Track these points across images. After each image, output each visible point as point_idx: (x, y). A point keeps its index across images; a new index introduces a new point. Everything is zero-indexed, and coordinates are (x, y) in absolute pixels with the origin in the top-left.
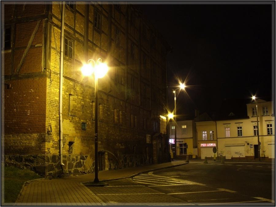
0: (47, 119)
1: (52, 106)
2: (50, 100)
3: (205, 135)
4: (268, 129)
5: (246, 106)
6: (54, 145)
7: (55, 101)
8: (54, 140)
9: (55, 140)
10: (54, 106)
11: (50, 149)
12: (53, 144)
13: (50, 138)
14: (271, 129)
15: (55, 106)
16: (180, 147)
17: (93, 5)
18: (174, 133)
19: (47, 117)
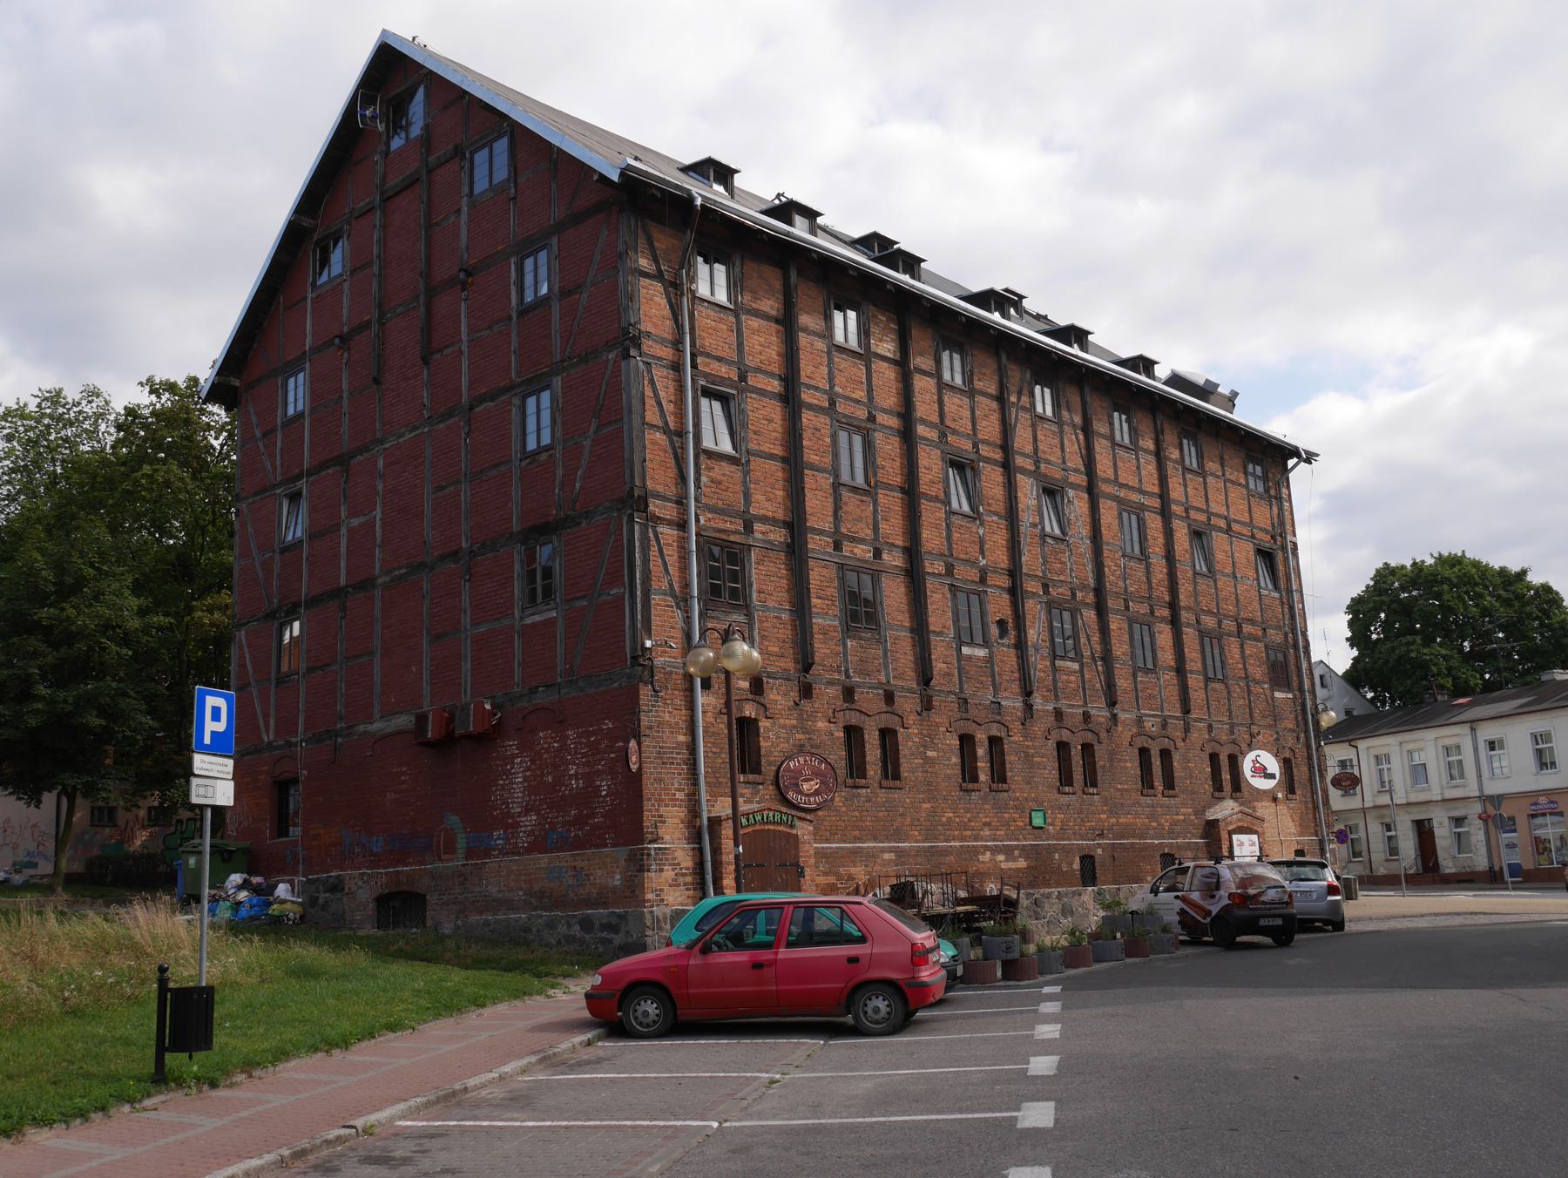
0: (647, 805)
1: (663, 763)
2: (655, 747)
3: (1019, 400)
4: (1381, 771)
5: (1041, 1164)
6: (681, 880)
7: (675, 748)
8: (679, 864)
9: (683, 865)
10: (673, 763)
11: (661, 890)
12: (676, 875)
13: (662, 859)
14: (1460, 762)
15: (678, 764)
16: (1400, 883)
17: (621, 430)
18: (728, 790)
19: (649, 799)
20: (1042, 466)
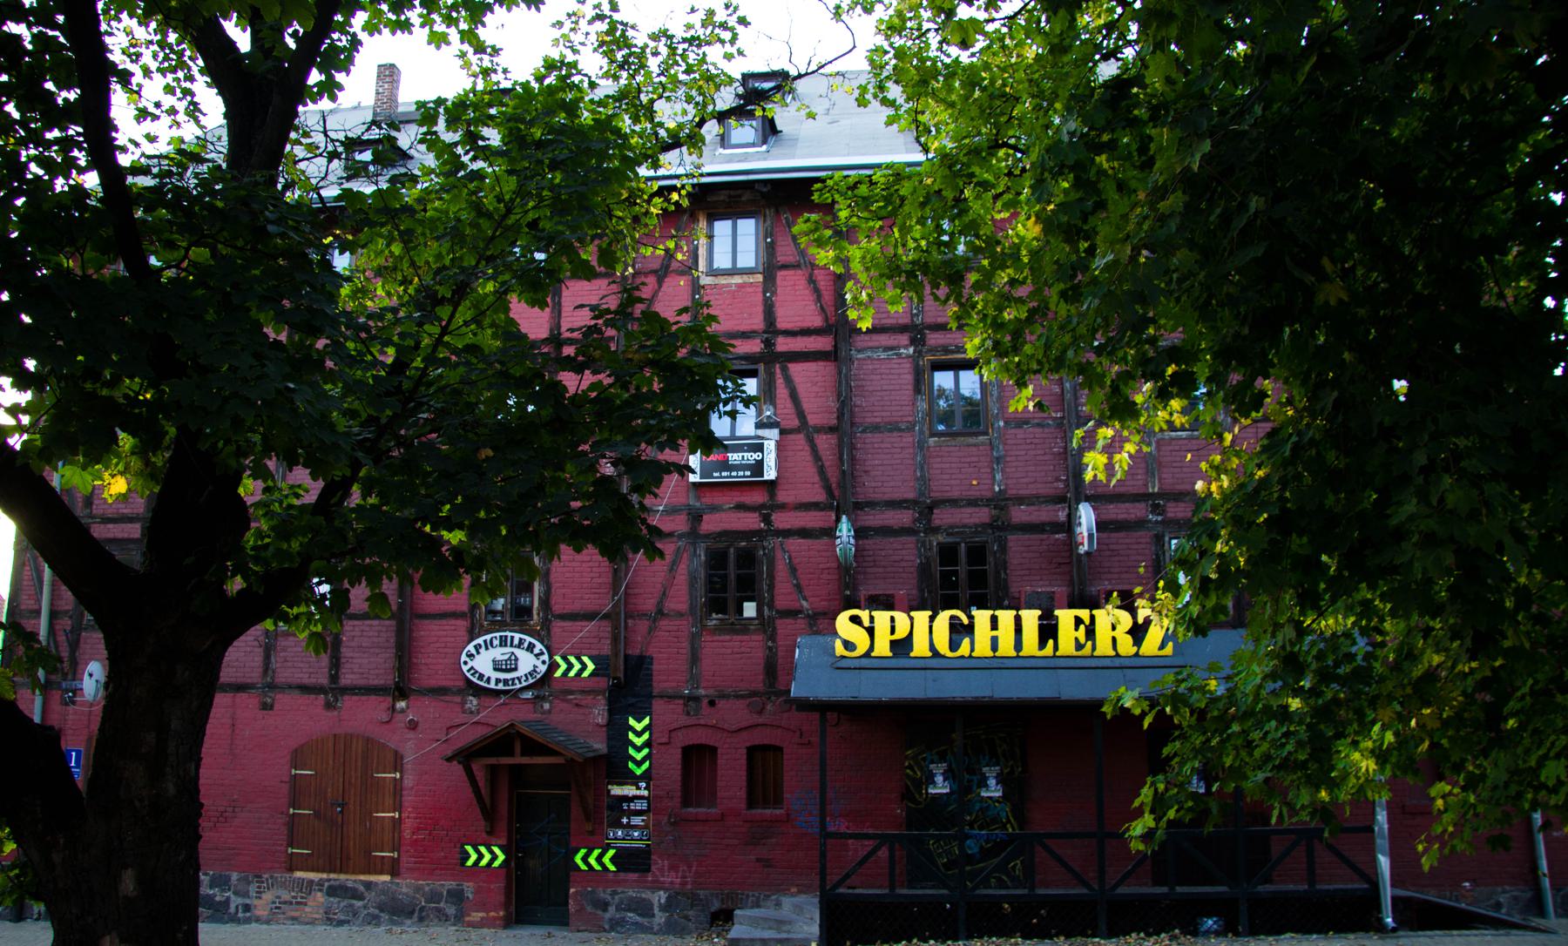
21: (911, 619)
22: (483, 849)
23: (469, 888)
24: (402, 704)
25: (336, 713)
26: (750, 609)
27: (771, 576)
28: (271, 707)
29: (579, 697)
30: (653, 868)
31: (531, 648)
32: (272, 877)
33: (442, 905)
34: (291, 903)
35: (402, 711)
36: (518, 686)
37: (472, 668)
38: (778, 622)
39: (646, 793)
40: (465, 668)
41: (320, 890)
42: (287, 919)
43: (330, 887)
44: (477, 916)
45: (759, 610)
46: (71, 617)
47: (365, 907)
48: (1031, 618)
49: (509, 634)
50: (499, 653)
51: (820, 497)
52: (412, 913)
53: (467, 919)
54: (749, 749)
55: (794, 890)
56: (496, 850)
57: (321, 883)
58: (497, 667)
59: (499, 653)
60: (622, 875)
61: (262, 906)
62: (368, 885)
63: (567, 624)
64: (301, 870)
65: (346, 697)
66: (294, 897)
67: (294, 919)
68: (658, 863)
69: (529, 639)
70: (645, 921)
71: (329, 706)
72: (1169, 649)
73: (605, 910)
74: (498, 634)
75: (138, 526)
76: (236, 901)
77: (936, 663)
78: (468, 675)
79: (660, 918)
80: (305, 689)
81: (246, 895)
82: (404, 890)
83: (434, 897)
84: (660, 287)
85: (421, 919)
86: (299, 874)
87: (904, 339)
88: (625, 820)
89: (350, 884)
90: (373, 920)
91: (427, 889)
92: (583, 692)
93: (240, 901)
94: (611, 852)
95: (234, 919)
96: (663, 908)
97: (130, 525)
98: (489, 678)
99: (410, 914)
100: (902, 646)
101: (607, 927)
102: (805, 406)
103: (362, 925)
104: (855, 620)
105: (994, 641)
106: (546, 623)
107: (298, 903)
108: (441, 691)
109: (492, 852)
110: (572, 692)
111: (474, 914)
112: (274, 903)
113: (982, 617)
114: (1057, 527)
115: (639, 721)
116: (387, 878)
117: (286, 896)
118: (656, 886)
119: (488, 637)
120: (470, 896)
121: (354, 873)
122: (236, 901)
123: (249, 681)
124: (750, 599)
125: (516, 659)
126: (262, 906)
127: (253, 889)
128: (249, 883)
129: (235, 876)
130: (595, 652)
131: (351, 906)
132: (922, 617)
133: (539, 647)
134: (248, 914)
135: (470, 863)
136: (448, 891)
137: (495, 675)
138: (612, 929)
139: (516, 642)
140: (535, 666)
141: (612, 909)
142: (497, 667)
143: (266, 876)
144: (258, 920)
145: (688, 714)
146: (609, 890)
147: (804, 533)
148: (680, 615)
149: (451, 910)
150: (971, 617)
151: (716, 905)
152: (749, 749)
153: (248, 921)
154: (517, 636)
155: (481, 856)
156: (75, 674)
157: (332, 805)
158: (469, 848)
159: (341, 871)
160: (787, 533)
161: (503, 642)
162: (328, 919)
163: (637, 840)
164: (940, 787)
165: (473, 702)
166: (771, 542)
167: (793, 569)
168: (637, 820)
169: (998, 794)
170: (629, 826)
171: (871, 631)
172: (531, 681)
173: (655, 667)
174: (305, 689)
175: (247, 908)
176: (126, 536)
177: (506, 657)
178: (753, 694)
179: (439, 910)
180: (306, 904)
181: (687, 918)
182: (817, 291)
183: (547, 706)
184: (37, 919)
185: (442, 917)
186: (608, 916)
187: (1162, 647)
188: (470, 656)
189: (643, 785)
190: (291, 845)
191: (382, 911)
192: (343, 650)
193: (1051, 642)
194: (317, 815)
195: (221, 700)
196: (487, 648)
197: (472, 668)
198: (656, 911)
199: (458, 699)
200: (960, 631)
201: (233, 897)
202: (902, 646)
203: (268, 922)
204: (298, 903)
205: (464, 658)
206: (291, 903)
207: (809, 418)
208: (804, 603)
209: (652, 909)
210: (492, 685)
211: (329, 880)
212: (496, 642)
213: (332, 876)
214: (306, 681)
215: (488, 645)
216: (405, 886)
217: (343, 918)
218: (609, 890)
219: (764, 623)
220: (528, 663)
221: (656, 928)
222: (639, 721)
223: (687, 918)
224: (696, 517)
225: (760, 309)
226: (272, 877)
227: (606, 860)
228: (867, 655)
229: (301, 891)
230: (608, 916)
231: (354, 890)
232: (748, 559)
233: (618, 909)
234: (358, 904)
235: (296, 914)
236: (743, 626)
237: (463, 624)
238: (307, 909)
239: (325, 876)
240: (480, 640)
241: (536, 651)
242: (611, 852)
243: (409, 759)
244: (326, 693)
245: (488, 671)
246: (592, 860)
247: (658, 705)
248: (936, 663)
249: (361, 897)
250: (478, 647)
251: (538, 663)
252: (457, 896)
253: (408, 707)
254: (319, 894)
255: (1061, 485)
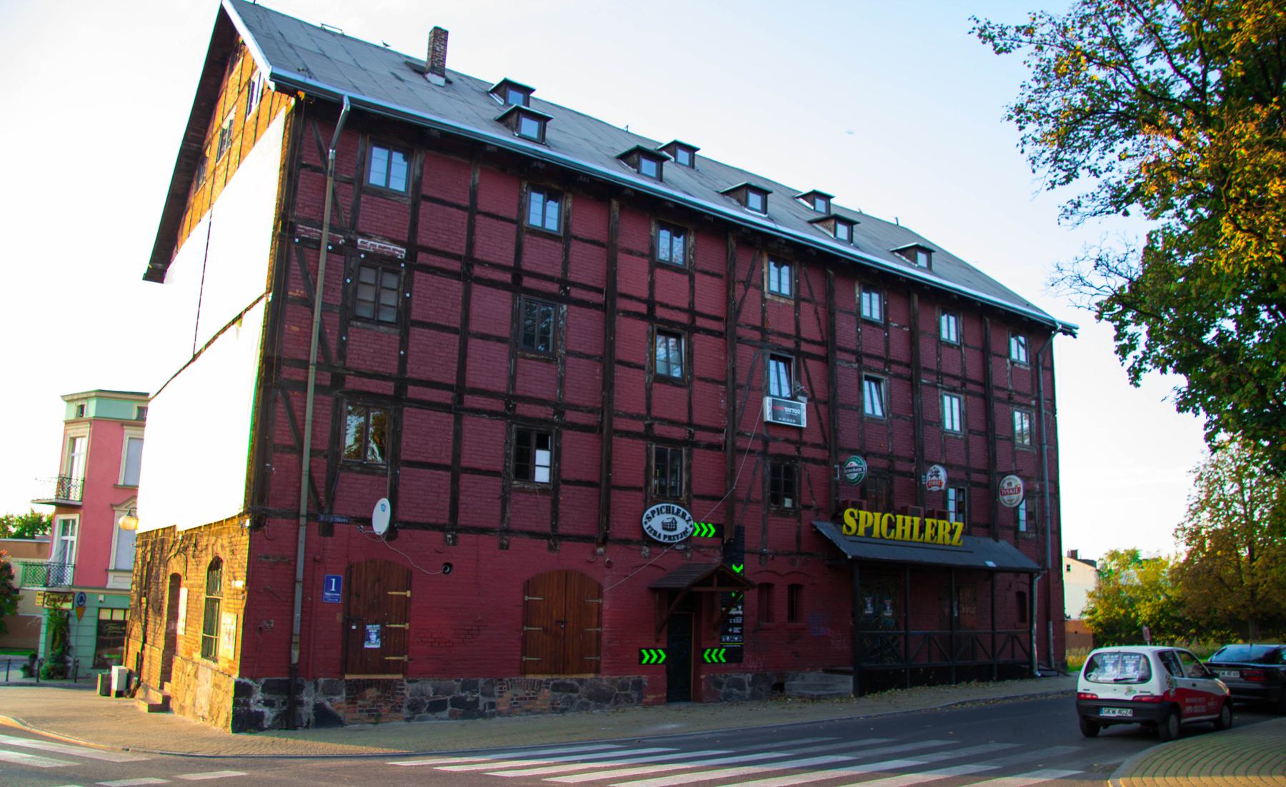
20: (803, 344)
21: (874, 517)
22: (652, 652)
23: (645, 678)
24: (601, 550)
25: (556, 554)
26: (788, 503)
27: (800, 484)
28: (507, 548)
29: (706, 550)
30: (744, 659)
31: (683, 516)
32: (511, 680)
33: (629, 692)
34: (526, 699)
35: (601, 554)
36: (677, 541)
37: (650, 527)
38: (803, 512)
39: (741, 613)
40: (645, 527)
41: (547, 688)
42: (523, 711)
43: (555, 684)
44: (650, 698)
45: (794, 504)
46: (326, 457)
47: (579, 697)
48: (917, 520)
49: (672, 505)
50: (665, 518)
51: (820, 441)
52: (610, 699)
53: (644, 700)
54: (789, 586)
55: (808, 669)
56: (661, 652)
57: (547, 683)
58: (665, 527)
59: (665, 518)
60: (729, 665)
61: (503, 702)
62: (581, 682)
63: (700, 502)
64: (533, 673)
65: (563, 543)
66: (528, 694)
67: (528, 711)
68: (746, 655)
69: (682, 510)
70: (741, 693)
71: (551, 548)
72: (961, 543)
73: (721, 688)
74: (665, 505)
75: (392, 384)
76: (483, 701)
77: (882, 541)
78: (647, 531)
79: (748, 690)
80: (533, 535)
81: (491, 695)
82: (605, 683)
83: (623, 687)
84: (746, 293)
85: (616, 703)
86: (530, 677)
87: (853, 358)
88: (730, 630)
89: (568, 682)
90: (584, 707)
91: (619, 681)
92: (708, 547)
93: (487, 700)
94: (723, 651)
95: (482, 715)
96: (750, 684)
97: (384, 383)
98: (660, 534)
99: (608, 700)
100: (869, 531)
101: (722, 698)
102: (814, 386)
103: (577, 710)
104: (852, 514)
105: (903, 531)
106: (688, 499)
107: (530, 699)
108: (626, 542)
109: (658, 653)
110: (702, 547)
111: (649, 697)
112: (512, 699)
113: (899, 517)
114: (911, 475)
115: (738, 566)
116: (591, 676)
117: (521, 693)
118: (746, 671)
119: (659, 506)
120: (646, 684)
121: (572, 673)
122: (483, 701)
123: (490, 525)
124: (789, 497)
125: (676, 523)
126: (503, 702)
127: (496, 690)
128: (493, 685)
129: (481, 682)
130: (716, 522)
131: (570, 697)
132: (877, 515)
133: (688, 515)
134: (493, 710)
135: (645, 661)
136: (633, 682)
137: (664, 533)
138: (725, 699)
139: (675, 511)
140: (687, 529)
141: (724, 686)
142: (665, 527)
143: (506, 679)
144: (500, 714)
145: (760, 563)
146: (723, 675)
147: (814, 461)
148: (758, 502)
149: (635, 695)
150: (896, 518)
151: (775, 681)
152: (789, 586)
153: (492, 715)
154: (676, 507)
155: (651, 656)
156: (331, 508)
157: (557, 622)
158: (644, 651)
159: (563, 673)
160: (807, 460)
161: (668, 510)
162: (554, 708)
163: (736, 642)
164: (869, 611)
165: (646, 551)
166: (800, 464)
167: (809, 482)
168: (736, 630)
169: (890, 614)
170: (733, 634)
171: (857, 521)
172: (684, 538)
173: (746, 533)
174: (533, 535)
175: (492, 705)
176: (380, 391)
177: (670, 521)
178: (791, 553)
179: (628, 696)
180: (536, 699)
181: (761, 690)
182: (818, 319)
183: (689, 555)
184: (307, 727)
185: (629, 699)
186: (722, 691)
187: (959, 542)
188: (649, 518)
189: (740, 607)
190: (524, 653)
191: (591, 699)
192: (560, 506)
193: (893, 531)
194: (545, 630)
195: (386, 152)
196: (659, 514)
197: (650, 527)
198: (747, 686)
199: (637, 547)
200: (892, 525)
201: (481, 697)
202: (869, 531)
203: (509, 714)
204: (530, 699)
205: (644, 520)
206: (526, 699)
207: (816, 393)
208: (814, 502)
209: (744, 686)
210: (661, 540)
211: (553, 680)
212: (664, 510)
213: (554, 676)
214: (534, 528)
215: (659, 512)
216: (605, 680)
217: (564, 707)
218: (723, 675)
219: (795, 512)
220: (682, 525)
221: (747, 697)
222: (738, 566)
223: (761, 690)
224: (766, 442)
225: (793, 322)
226: (511, 680)
227: (720, 656)
228: (855, 535)
229: (533, 689)
230: (722, 691)
231: (572, 685)
232: (789, 471)
233: (728, 686)
234: (574, 695)
235: (528, 707)
236: (784, 513)
237: (640, 495)
238: (538, 702)
239: (549, 677)
240: (654, 508)
241: (687, 518)
242: (723, 651)
243: (606, 590)
244: (548, 539)
245: (659, 529)
246: (713, 656)
247: (747, 557)
248: (882, 541)
249: (576, 691)
250: (653, 512)
251: (688, 526)
252: (638, 685)
253: (605, 552)
254: (546, 691)
255: (912, 453)
